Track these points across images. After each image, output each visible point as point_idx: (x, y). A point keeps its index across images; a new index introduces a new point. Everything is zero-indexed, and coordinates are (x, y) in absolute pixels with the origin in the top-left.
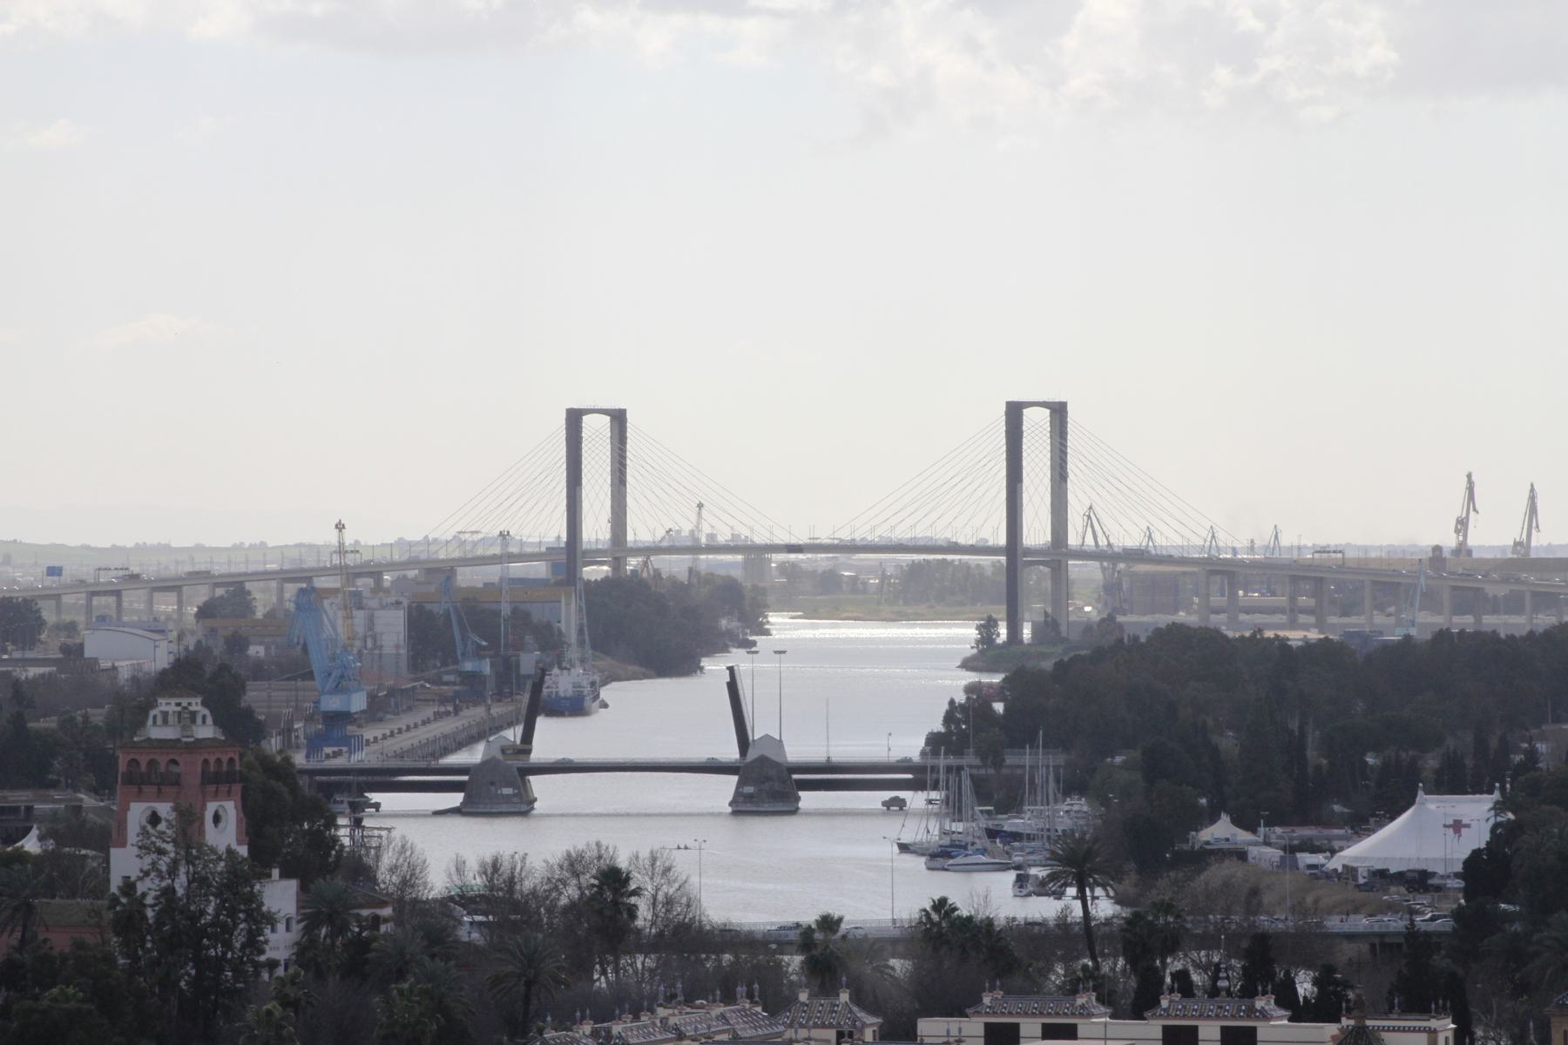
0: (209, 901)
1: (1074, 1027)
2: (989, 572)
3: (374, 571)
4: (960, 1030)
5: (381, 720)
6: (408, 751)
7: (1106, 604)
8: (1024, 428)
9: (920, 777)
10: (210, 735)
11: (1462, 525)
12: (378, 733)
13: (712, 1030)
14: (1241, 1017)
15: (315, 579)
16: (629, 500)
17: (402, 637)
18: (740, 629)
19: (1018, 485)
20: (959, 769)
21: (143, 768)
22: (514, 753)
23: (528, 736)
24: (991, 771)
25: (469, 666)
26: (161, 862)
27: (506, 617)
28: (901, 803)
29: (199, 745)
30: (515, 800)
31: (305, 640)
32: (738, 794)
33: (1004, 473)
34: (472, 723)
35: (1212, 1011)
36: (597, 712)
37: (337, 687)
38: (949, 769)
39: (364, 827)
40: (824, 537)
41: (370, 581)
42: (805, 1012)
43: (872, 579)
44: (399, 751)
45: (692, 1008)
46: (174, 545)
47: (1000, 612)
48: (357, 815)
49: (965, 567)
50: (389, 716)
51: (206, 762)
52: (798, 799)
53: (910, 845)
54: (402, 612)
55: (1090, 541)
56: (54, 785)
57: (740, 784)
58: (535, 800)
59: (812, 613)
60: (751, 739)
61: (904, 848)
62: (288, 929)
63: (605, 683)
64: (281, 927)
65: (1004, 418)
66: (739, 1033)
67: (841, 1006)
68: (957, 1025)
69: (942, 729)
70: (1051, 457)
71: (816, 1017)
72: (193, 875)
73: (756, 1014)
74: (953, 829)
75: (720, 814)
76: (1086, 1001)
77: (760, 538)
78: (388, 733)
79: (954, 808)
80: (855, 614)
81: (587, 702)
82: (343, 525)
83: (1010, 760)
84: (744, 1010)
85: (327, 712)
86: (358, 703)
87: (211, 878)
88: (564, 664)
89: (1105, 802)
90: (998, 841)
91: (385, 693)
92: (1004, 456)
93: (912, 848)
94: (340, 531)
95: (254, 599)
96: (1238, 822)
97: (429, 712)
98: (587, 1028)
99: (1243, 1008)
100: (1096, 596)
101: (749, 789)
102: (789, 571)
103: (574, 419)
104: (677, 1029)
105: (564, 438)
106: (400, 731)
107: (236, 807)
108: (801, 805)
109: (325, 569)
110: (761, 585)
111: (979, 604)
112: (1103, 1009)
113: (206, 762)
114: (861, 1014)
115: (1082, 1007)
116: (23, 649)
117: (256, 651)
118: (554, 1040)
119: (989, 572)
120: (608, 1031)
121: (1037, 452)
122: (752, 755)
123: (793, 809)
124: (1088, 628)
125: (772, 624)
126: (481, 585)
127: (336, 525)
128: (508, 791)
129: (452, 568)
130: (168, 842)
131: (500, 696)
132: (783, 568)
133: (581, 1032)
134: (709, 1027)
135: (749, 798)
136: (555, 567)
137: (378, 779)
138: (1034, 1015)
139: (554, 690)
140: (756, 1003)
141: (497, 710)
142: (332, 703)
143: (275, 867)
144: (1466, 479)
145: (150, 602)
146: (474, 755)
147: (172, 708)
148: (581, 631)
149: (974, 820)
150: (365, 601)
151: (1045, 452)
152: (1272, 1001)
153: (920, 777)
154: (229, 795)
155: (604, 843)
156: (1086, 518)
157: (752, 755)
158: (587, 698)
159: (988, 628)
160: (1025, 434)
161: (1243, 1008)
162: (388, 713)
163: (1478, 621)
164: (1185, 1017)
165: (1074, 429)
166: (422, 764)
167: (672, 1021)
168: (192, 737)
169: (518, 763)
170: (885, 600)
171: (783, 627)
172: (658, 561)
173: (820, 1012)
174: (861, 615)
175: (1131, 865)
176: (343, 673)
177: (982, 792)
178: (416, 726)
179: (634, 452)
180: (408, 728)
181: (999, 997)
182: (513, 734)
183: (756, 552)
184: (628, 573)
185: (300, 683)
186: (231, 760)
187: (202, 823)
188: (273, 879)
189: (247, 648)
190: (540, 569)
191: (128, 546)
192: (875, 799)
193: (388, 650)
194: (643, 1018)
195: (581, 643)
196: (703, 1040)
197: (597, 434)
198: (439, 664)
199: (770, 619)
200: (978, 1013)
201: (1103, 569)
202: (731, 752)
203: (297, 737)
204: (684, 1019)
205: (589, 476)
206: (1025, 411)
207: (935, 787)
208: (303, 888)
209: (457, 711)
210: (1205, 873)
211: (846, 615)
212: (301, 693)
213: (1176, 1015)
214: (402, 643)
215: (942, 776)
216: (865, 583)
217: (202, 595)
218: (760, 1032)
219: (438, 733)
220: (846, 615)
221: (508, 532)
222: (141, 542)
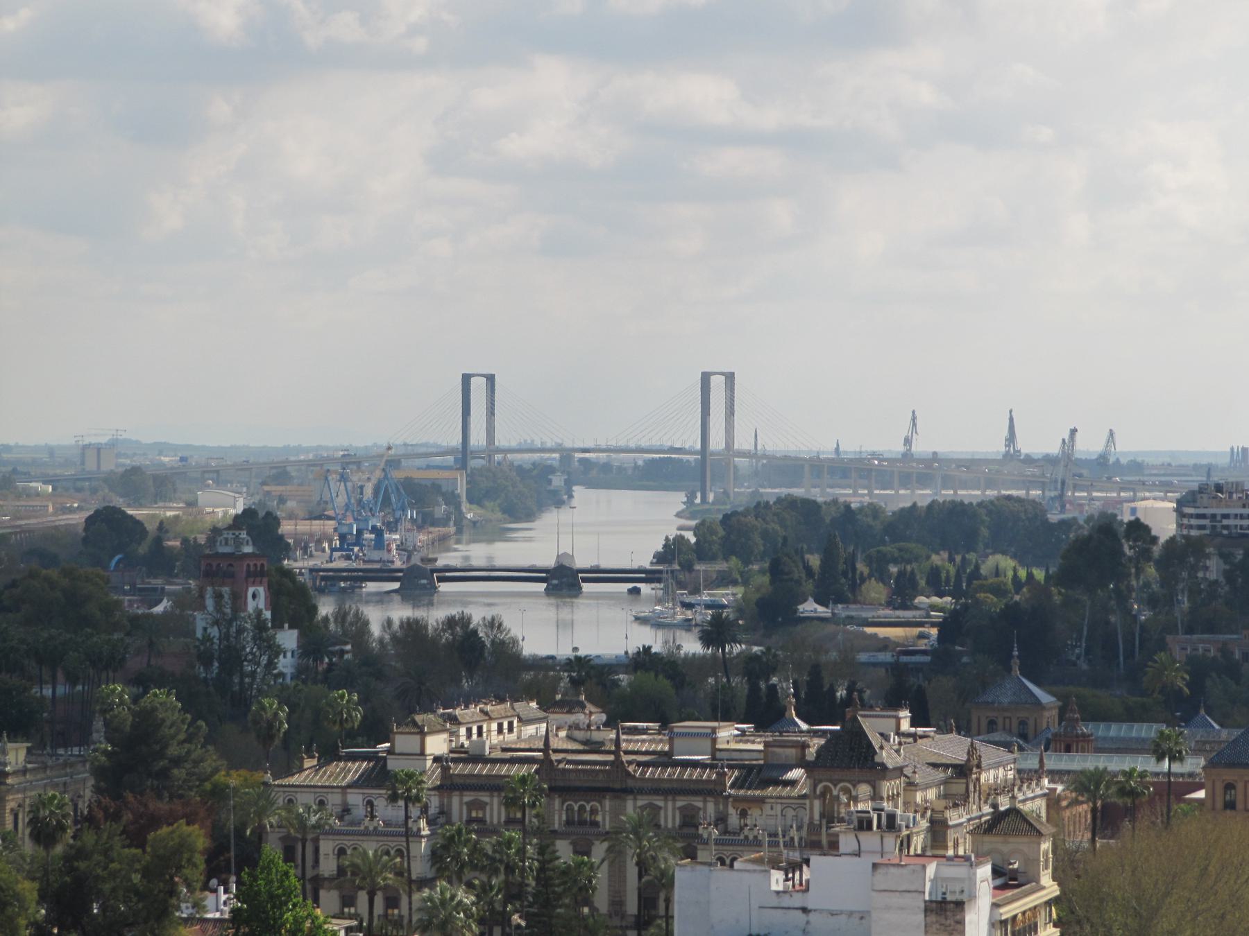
9: (650, 576)
11: (908, 441)
21: (214, 568)
40: (603, 444)
49: (681, 460)
51: (248, 565)
56: (177, 576)
62: (293, 656)
64: (289, 655)
77: (568, 444)
96: (818, 602)
103: (466, 379)
107: (265, 590)
113: (248, 565)
116: (165, 501)
128: (424, 581)
132: (581, 460)
136: (456, 460)
144: (911, 414)
153: (650, 576)
154: (261, 583)
163: (1028, 493)
186: (262, 565)
187: (246, 598)
191: (292, 445)
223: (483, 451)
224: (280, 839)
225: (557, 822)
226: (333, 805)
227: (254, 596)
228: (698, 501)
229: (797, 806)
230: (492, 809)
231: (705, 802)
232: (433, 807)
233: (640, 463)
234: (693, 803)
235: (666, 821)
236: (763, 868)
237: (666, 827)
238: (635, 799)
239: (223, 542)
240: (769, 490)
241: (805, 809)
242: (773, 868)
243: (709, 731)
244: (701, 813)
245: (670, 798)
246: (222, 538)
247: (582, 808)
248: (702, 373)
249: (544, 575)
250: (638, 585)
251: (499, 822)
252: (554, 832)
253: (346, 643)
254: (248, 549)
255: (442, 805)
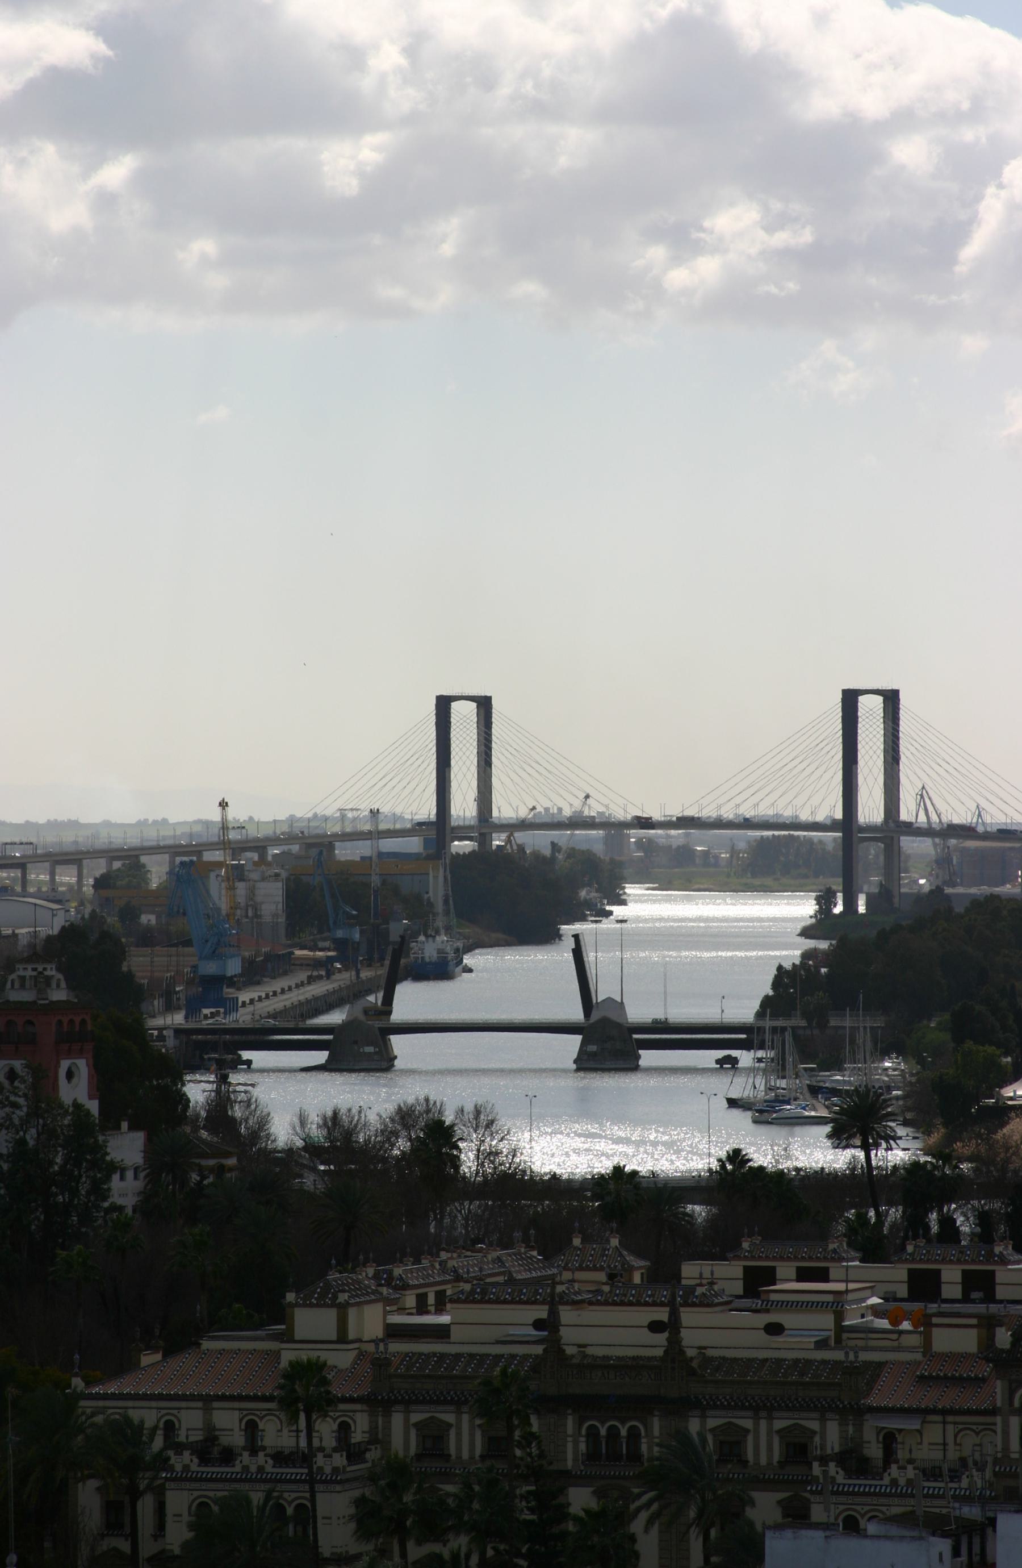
0: (57, 1152)
1: (827, 1269)
2: (830, 847)
3: (260, 846)
4: (712, 1273)
5: (258, 983)
6: (281, 1012)
7: (937, 877)
8: (859, 714)
10: (64, 998)
12: (255, 995)
13: (484, 1273)
14: (980, 1261)
15: (205, 853)
16: (495, 781)
17: (280, 906)
18: (598, 900)
19: (854, 766)
20: (783, 1029)
22: (375, 1015)
23: (388, 1000)
24: (816, 1032)
25: (340, 934)
26: (14, 1116)
27: (376, 888)
28: (734, 1061)
29: (55, 1007)
30: (376, 1057)
31: (184, 910)
32: (582, 1051)
33: (840, 755)
34: (343, 986)
35: (954, 1255)
36: (461, 975)
37: (214, 952)
38: (774, 1030)
39: (230, 1083)
41: (255, 857)
42: (578, 1255)
43: (723, 853)
44: (272, 1011)
45: (473, 1252)
46: (82, 821)
47: (837, 884)
48: (223, 1072)
49: (809, 841)
50: (265, 980)
51: (60, 1022)
52: (639, 1057)
53: (738, 1100)
54: (280, 884)
55: (922, 818)
57: (583, 1044)
58: (396, 1057)
59: (666, 884)
60: (594, 1001)
61: (732, 1103)
62: (136, 1178)
63: (469, 949)
64: (130, 1174)
65: (840, 704)
66: (515, 1275)
67: (611, 1250)
68: (710, 1268)
69: (771, 993)
70: (884, 740)
71: (589, 1261)
72: (43, 1127)
73: (531, 1257)
74: (778, 1085)
75: (565, 1071)
76: (838, 1247)
77: (621, 813)
78: (264, 996)
79: (779, 1067)
80: (706, 886)
81: (451, 967)
82: (227, 803)
83: (833, 1023)
84: (520, 1254)
85: (204, 976)
86: (233, 967)
87: (59, 1130)
88: (430, 932)
89: (921, 1061)
90: (820, 1096)
91: (262, 958)
92: (841, 740)
93: (740, 1103)
94: (224, 809)
95: (149, 871)
97: (303, 976)
98: (371, 1271)
99: (983, 1252)
100: (929, 869)
101: (592, 1048)
102: (648, 846)
104: (455, 1270)
105: (434, 723)
106: (275, 994)
107: (88, 1065)
108: (642, 1063)
109: (212, 844)
110: (617, 858)
111: (821, 877)
112: (853, 1254)
113: (60, 1022)
114: (630, 1258)
115: (834, 1251)
117: (148, 919)
118: (336, 1281)
119: (830, 847)
120: (390, 1273)
121: (871, 736)
122: (595, 1016)
123: (633, 1066)
124: (919, 898)
125: (629, 895)
126: (359, 859)
127: (220, 803)
129: (330, 843)
130: (20, 1096)
131: (369, 963)
133: (364, 1274)
134: (481, 1270)
135: (593, 1056)
136: (426, 843)
137: (251, 1038)
138: (789, 1259)
139: (420, 956)
140: (533, 1248)
141: (366, 974)
142: (210, 968)
143: (124, 1120)
145: (52, 874)
146: (336, 1017)
147: (29, 973)
148: (446, 902)
149: (797, 1076)
150: (246, 873)
151: (878, 736)
152: (1010, 1247)
154: (80, 1054)
155: (432, 1098)
156: (919, 797)
157: (595, 1016)
158: (451, 963)
159: (825, 900)
160: (860, 720)
161: (983, 1252)
162: (264, 976)
164: (928, 1261)
165: (498, 718)
166: (291, 1025)
167: (451, 1264)
168: (47, 999)
169: (378, 1024)
170: (735, 873)
171: (639, 899)
172: (520, 837)
173: (592, 1255)
174: (711, 886)
175: (938, 1121)
176: (219, 941)
177: (806, 1054)
178: (290, 989)
179: (498, 736)
180: (283, 991)
181: (758, 1242)
182: (375, 999)
183: (615, 828)
184: (494, 848)
185: (180, 949)
186: (83, 1022)
188: (122, 1131)
189: (139, 917)
190: (414, 845)
191: (40, 822)
192: (709, 1057)
193: (267, 919)
194: (423, 1261)
195: (447, 913)
196: (475, 1282)
197: (465, 719)
198: (315, 932)
199: (627, 891)
200: (738, 1258)
201: (935, 845)
202: (575, 1013)
203: (178, 999)
204: (462, 1262)
205: (457, 758)
206: (861, 698)
207: (762, 1047)
208: (149, 1140)
209: (328, 976)
210: (1008, 1127)
211: (697, 886)
212: (181, 958)
213: (921, 1259)
214: (280, 912)
215: (767, 1036)
216: (717, 857)
217: (99, 868)
218: (534, 1274)
219: (309, 996)
220: (697, 886)
221: (378, 810)
222: (52, 819)
223: (470, 828)
224: (779, 1502)
225: (570, 1456)
226: (188, 1430)
227: (70, 1075)
228: (838, 909)
229: (981, 1427)
230: (459, 1434)
231: (823, 1420)
232: (359, 1431)
233: (742, 845)
234: (437, 1415)
235: (459, 1448)
236: (915, 1534)
237: (459, 1457)
238: (407, 1412)
239: (17, 985)
240: (960, 890)
241: (995, 1432)
242: (934, 1535)
243: (830, 1298)
244: (817, 1439)
245: (763, 1414)
246: (13, 976)
247: (613, 1433)
248: (490, 698)
249: (744, 1036)
250: (734, 1053)
251: (472, 1458)
252: (565, 1474)
253: (227, 1155)
254: (59, 995)
255: (373, 1430)
